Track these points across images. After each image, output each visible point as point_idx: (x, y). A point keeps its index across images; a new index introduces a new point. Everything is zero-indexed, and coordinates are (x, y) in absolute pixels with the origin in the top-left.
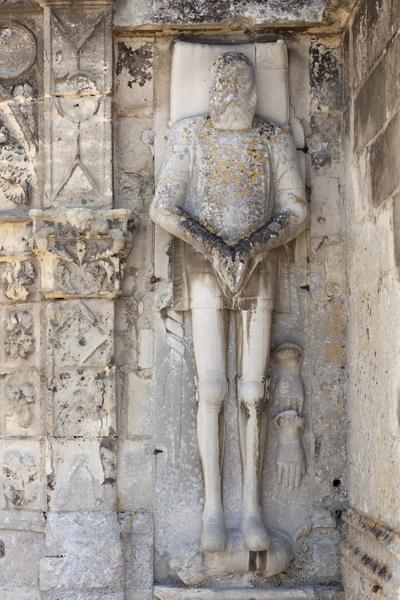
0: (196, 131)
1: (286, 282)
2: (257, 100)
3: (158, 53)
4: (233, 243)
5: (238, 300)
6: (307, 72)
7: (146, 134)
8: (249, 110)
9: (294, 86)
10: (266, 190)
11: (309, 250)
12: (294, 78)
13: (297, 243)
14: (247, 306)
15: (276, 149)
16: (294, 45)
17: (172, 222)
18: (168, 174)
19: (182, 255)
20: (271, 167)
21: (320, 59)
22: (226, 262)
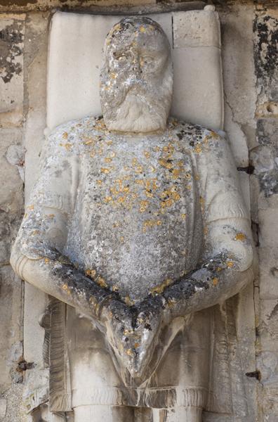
0: (81, 137)
1: (224, 365)
2: (174, 87)
3: (32, 34)
4: (135, 302)
5: (145, 391)
6: (250, 57)
7: (12, 151)
8: (161, 101)
9: (231, 77)
10: (188, 219)
11: (258, 317)
12: (232, 66)
13: (240, 301)
14: (160, 400)
15: (203, 160)
16: (231, 18)
17: (42, 272)
18: (40, 200)
19: (62, 326)
20: (196, 186)
21: (270, 38)
22: (123, 329)
